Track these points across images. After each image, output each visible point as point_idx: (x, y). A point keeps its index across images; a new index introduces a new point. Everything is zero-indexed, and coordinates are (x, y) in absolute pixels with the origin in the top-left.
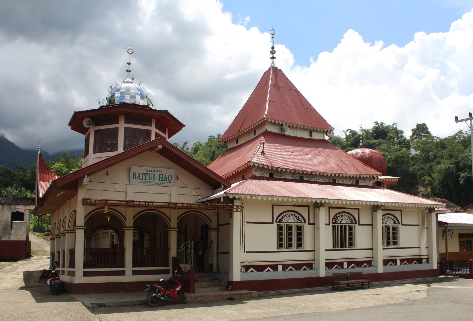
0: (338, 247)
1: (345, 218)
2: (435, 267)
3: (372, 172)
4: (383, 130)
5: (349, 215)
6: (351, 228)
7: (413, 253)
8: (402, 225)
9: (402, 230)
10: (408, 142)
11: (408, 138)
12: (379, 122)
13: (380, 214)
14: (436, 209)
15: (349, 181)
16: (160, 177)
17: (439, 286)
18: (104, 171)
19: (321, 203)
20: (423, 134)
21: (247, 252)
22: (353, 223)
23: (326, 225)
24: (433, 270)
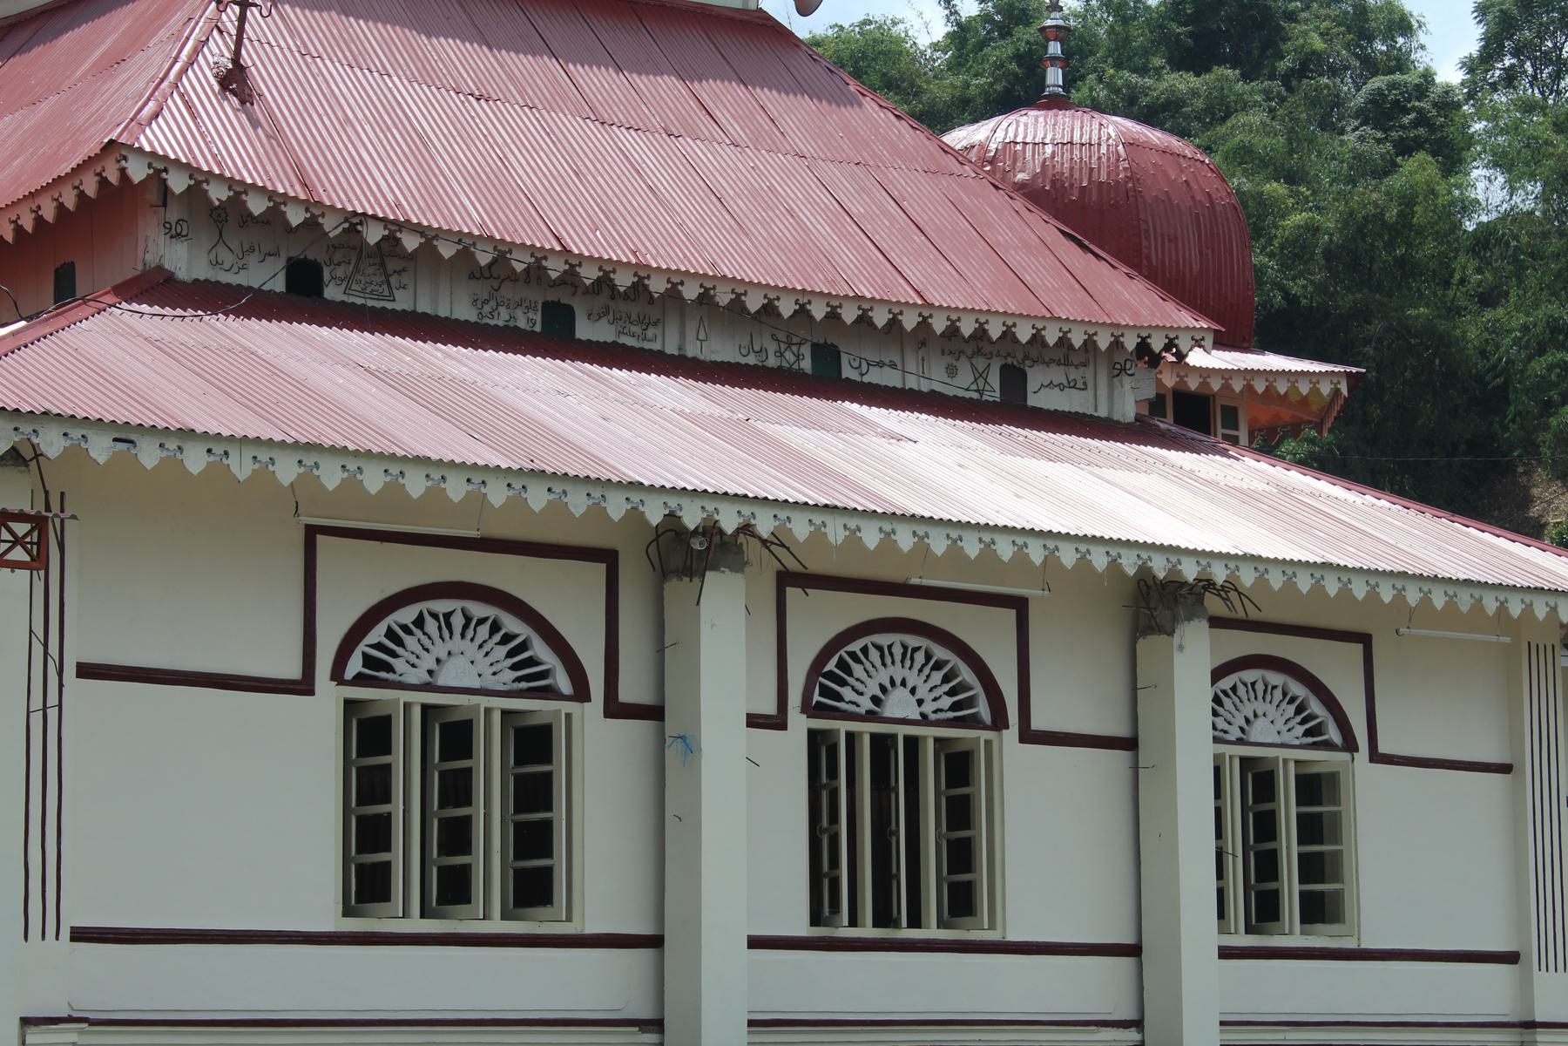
0: (853, 922)
5: (940, 653)
6: (958, 766)
8: (1376, 757)
9: (1376, 804)
11: (1449, 74)
13: (1193, 654)
15: (952, 371)
19: (710, 530)
21: (80, 935)
22: (973, 722)
23: (754, 721)
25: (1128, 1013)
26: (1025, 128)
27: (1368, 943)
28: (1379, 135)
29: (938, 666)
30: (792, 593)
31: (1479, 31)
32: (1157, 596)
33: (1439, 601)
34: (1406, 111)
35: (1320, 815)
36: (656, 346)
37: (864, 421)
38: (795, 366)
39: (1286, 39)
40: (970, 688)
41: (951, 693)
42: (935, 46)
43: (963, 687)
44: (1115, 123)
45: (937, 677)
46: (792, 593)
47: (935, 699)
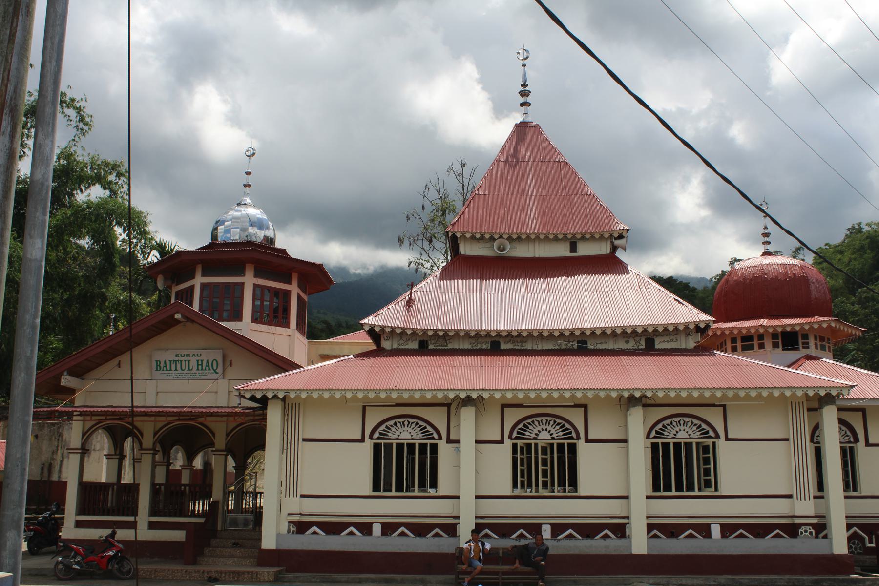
8: (727, 439)
16: (198, 365)
18: (115, 362)
21: (302, 496)
29: (558, 424)
43: (567, 429)
45: (695, 428)
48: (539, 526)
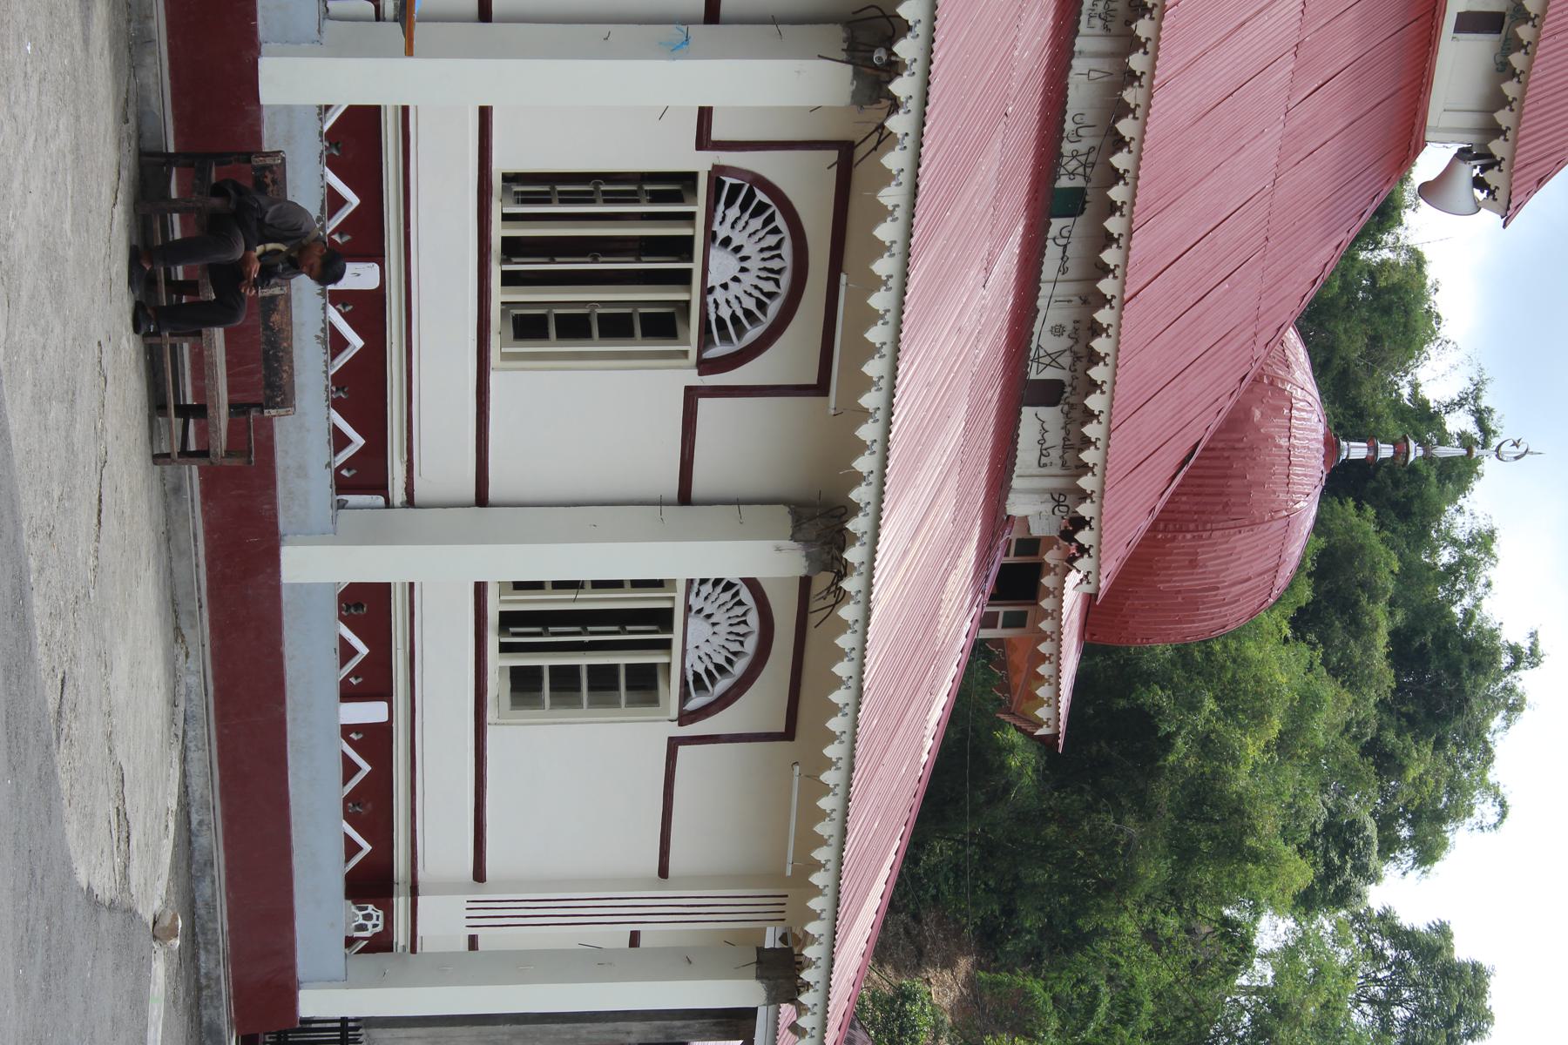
0: (506, 217)
1: (748, 280)
2: (314, 1003)
3: (1122, 517)
4: (1460, 703)
5: (774, 307)
6: (662, 325)
7: (436, 834)
8: (674, 744)
9: (626, 741)
10: (1342, 897)
11: (1377, 897)
12: (1526, 681)
13: (771, 559)
14: (787, 1010)
15: (1058, 331)
17: (157, 1009)
19: (894, 68)
20: (1400, 1013)
22: (705, 340)
23: (705, 115)
24: (286, 991)
25: (419, 495)
26: (1308, 415)
27: (491, 732)
28: (1319, 827)
29: (761, 306)
30: (833, 155)
31: (1421, 926)
32: (824, 522)
33: (826, 803)
34: (1342, 856)
35: (617, 688)
36: (1083, 28)
37: (1005, 236)
38: (1062, 171)
39: (1416, 740)
40: (739, 336)
41: (734, 317)
42: (1415, 386)
43: (740, 331)
44: (1309, 509)
45: (750, 304)
46: (833, 155)
47: (728, 302)
48: (375, 254)
